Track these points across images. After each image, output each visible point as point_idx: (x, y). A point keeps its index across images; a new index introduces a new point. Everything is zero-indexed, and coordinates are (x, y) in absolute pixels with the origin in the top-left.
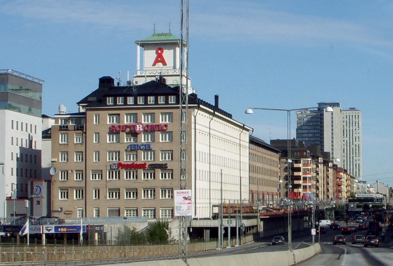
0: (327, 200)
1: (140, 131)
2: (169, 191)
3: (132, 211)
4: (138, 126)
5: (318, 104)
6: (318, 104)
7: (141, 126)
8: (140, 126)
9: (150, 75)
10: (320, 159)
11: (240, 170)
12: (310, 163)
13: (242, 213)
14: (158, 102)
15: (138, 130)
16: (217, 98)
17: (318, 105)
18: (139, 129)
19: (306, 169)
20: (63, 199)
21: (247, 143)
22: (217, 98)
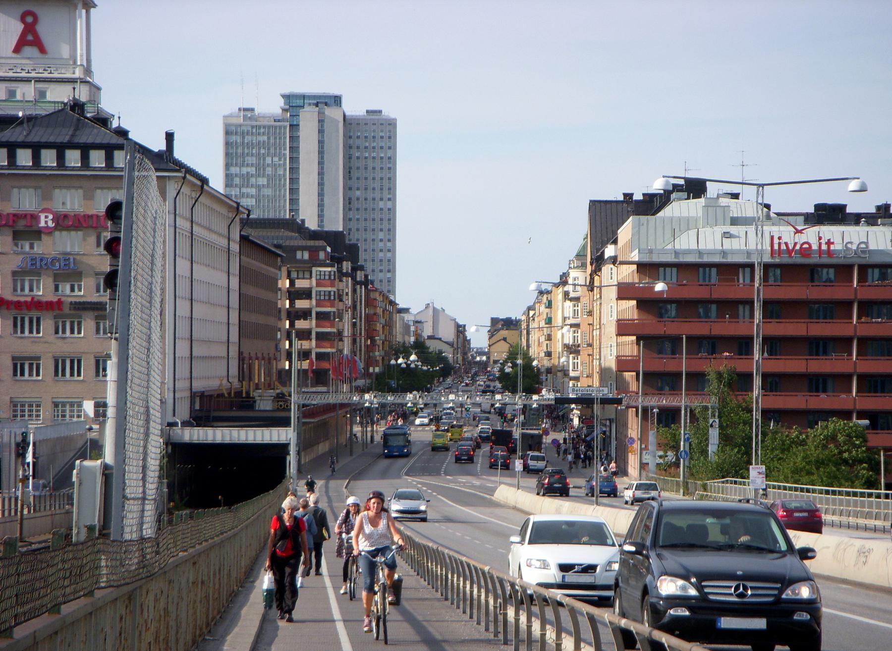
0: (27, 427)
1: (48, 226)
2: (31, 365)
3: (68, 406)
4: (42, 216)
5: (283, 96)
6: (283, 96)
7: (51, 217)
8: (46, 217)
9: (11, 74)
10: (345, 263)
11: (228, 308)
12: (335, 279)
13: (751, 303)
14: (112, 163)
15: (42, 224)
16: (170, 137)
17: (281, 102)
18: (46, 222)
19: (330, 292)
20: (35, 378)
21: (236, 242)
22: (170, 137)
